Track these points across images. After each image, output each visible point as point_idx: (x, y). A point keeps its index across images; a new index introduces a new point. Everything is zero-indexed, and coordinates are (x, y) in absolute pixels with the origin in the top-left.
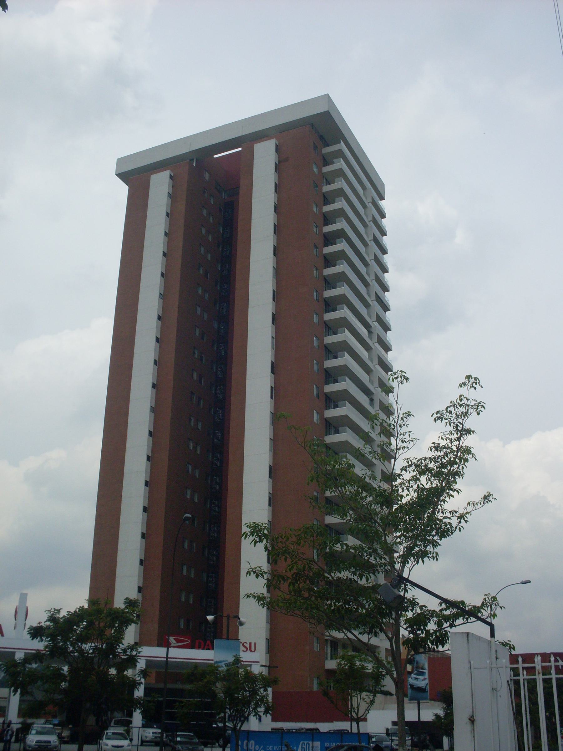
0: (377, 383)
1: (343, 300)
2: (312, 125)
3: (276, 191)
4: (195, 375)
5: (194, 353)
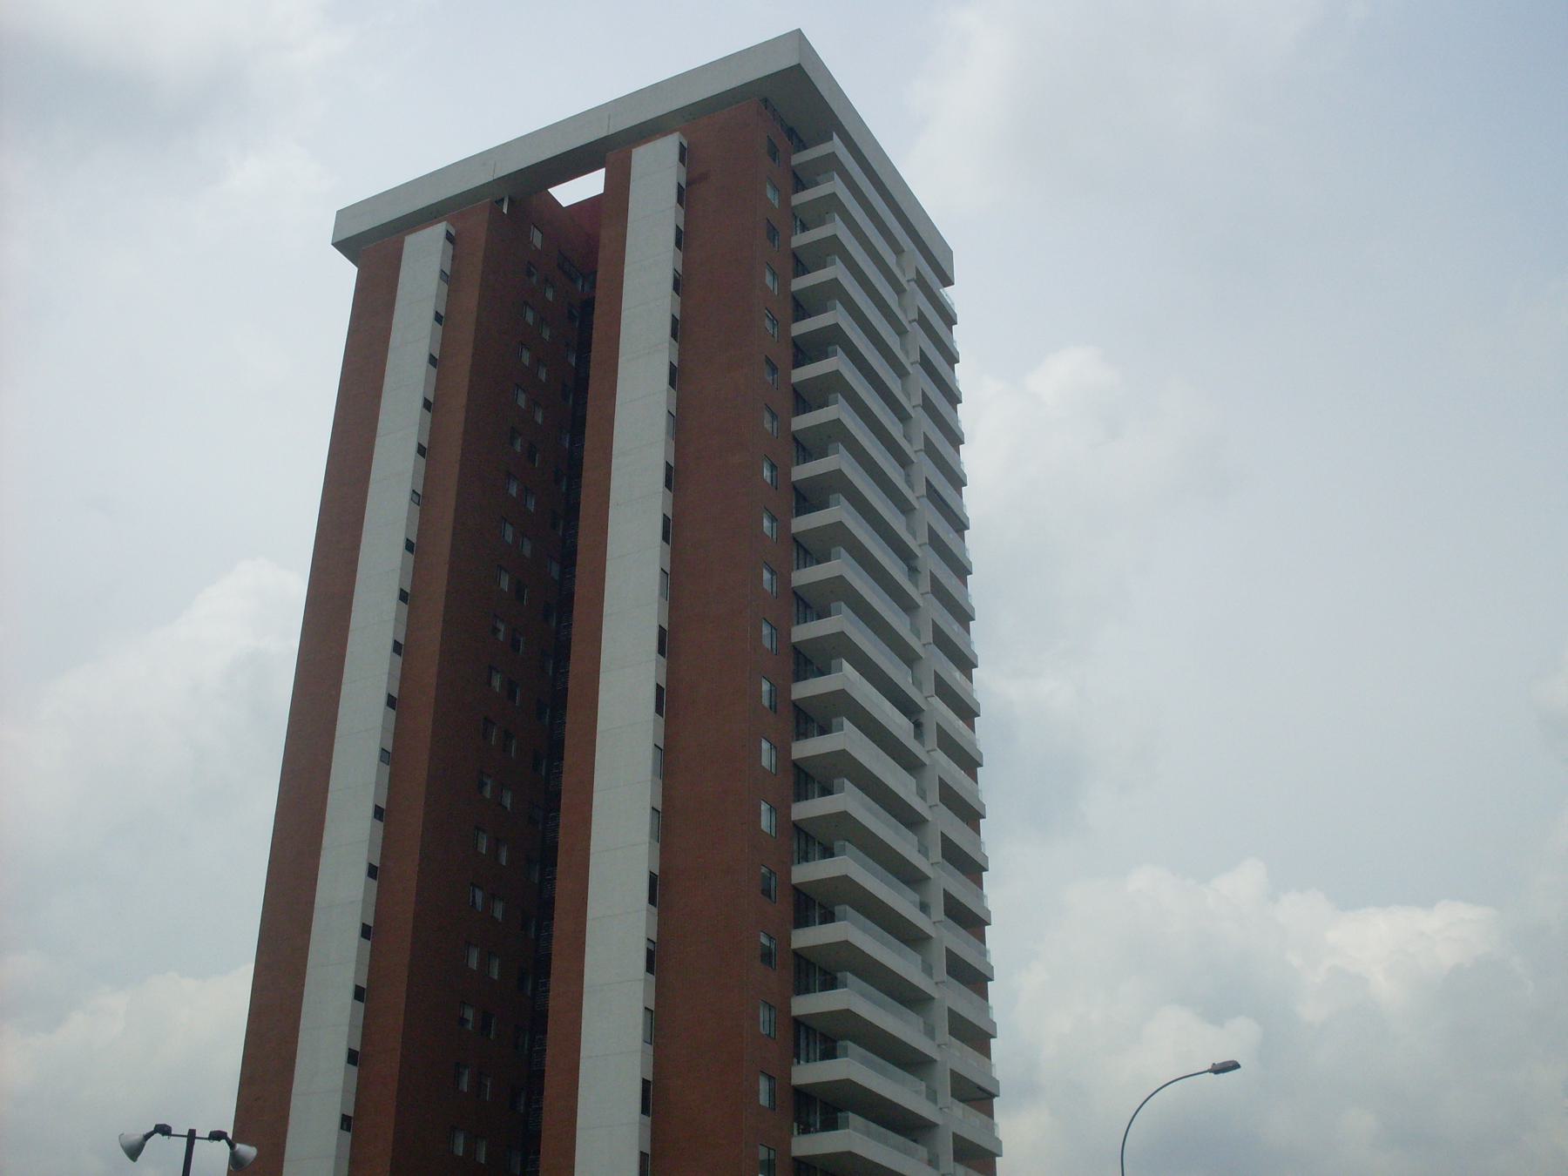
0: (930, 686)
1: (836, 484)
2: (766, 100)
3: (652, 900)
4: (497, 682)
5: (495, 630)
